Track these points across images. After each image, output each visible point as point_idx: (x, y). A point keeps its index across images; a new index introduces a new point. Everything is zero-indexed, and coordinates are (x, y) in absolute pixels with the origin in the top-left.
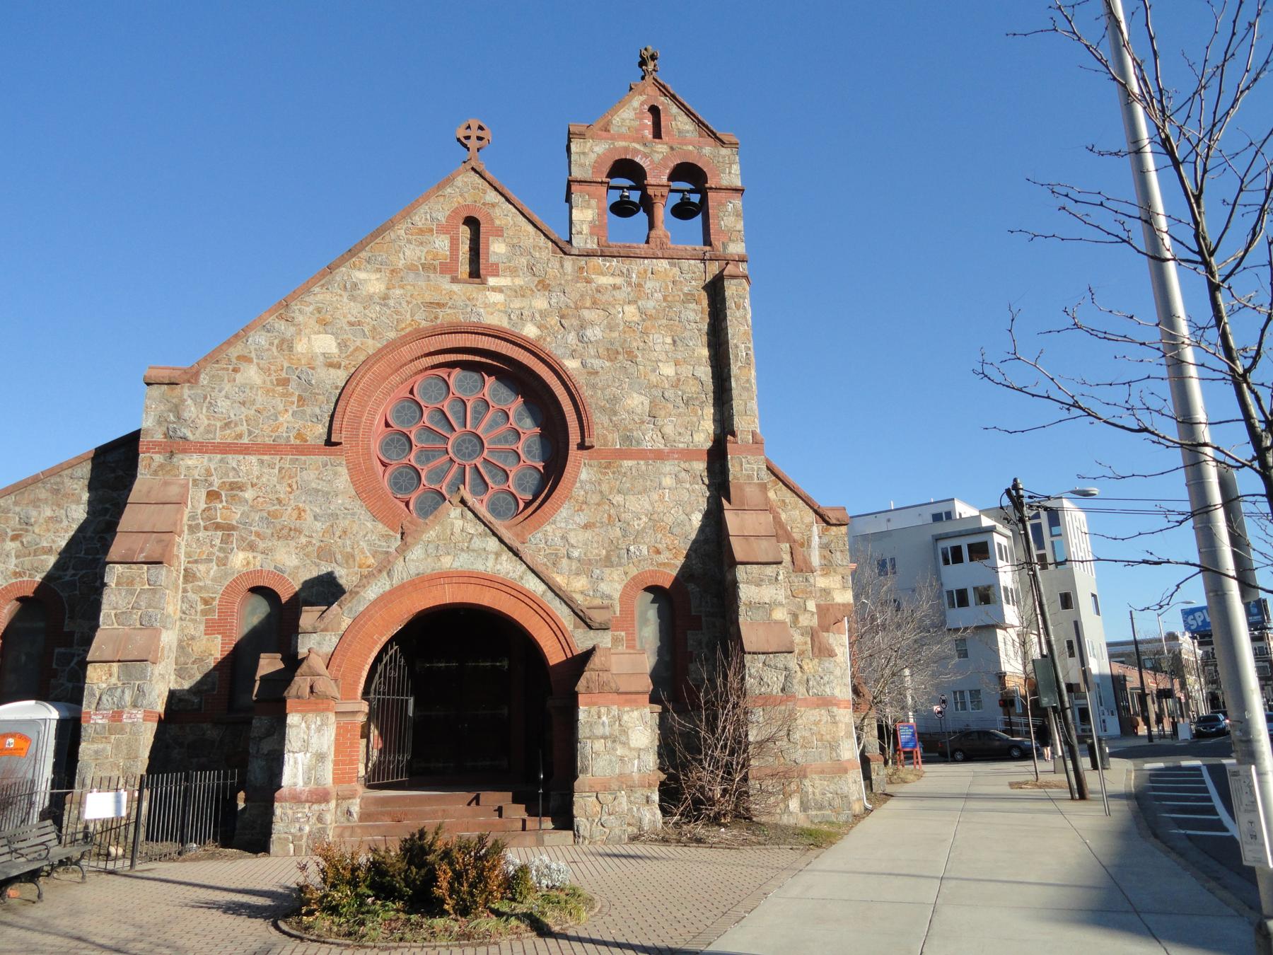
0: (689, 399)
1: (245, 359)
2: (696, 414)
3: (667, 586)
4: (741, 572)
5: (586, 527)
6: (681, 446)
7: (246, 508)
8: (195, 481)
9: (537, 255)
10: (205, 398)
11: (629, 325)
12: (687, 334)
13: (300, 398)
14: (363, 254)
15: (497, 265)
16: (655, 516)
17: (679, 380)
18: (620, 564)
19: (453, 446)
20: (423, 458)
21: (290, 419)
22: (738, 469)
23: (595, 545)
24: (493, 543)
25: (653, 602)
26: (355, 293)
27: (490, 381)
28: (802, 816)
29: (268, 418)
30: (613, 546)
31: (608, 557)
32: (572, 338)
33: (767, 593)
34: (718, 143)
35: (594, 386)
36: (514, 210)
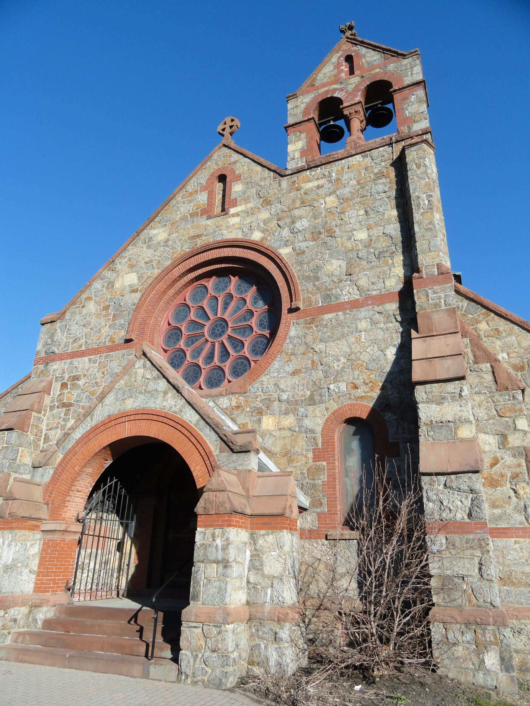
0: (380, 253)
1: (89, 299)
2: (387, 264)
3: (364, 416)
4: (420, 393)
5: (295, 373)
6: (374, 293)
7: (79, 391)
8: (56, 378)
9: (263, 183)
10: (66, 326)
11: (329, 211)
12: (378, 203)
13: (114, 315)
14: (157, 219)
15: (236, 199)
16: (353, 356)
17: (371, 240)
18: (321, 402)
19: (209, 331)
20: (190, 343)
21: (108, 330)
22: (424, 299)
23: (301, 388)
24: (163, 384)
25: (355, 434)
26: (150, 244)
27: (234, 280)
28: (503, 677)
29: (96, 332)
30: (316, 386)
31: (312, 397)
32: (286, 232)
33: (449, 411)
34: (400, 58)
35: (301, 263)
36: (249, 160)
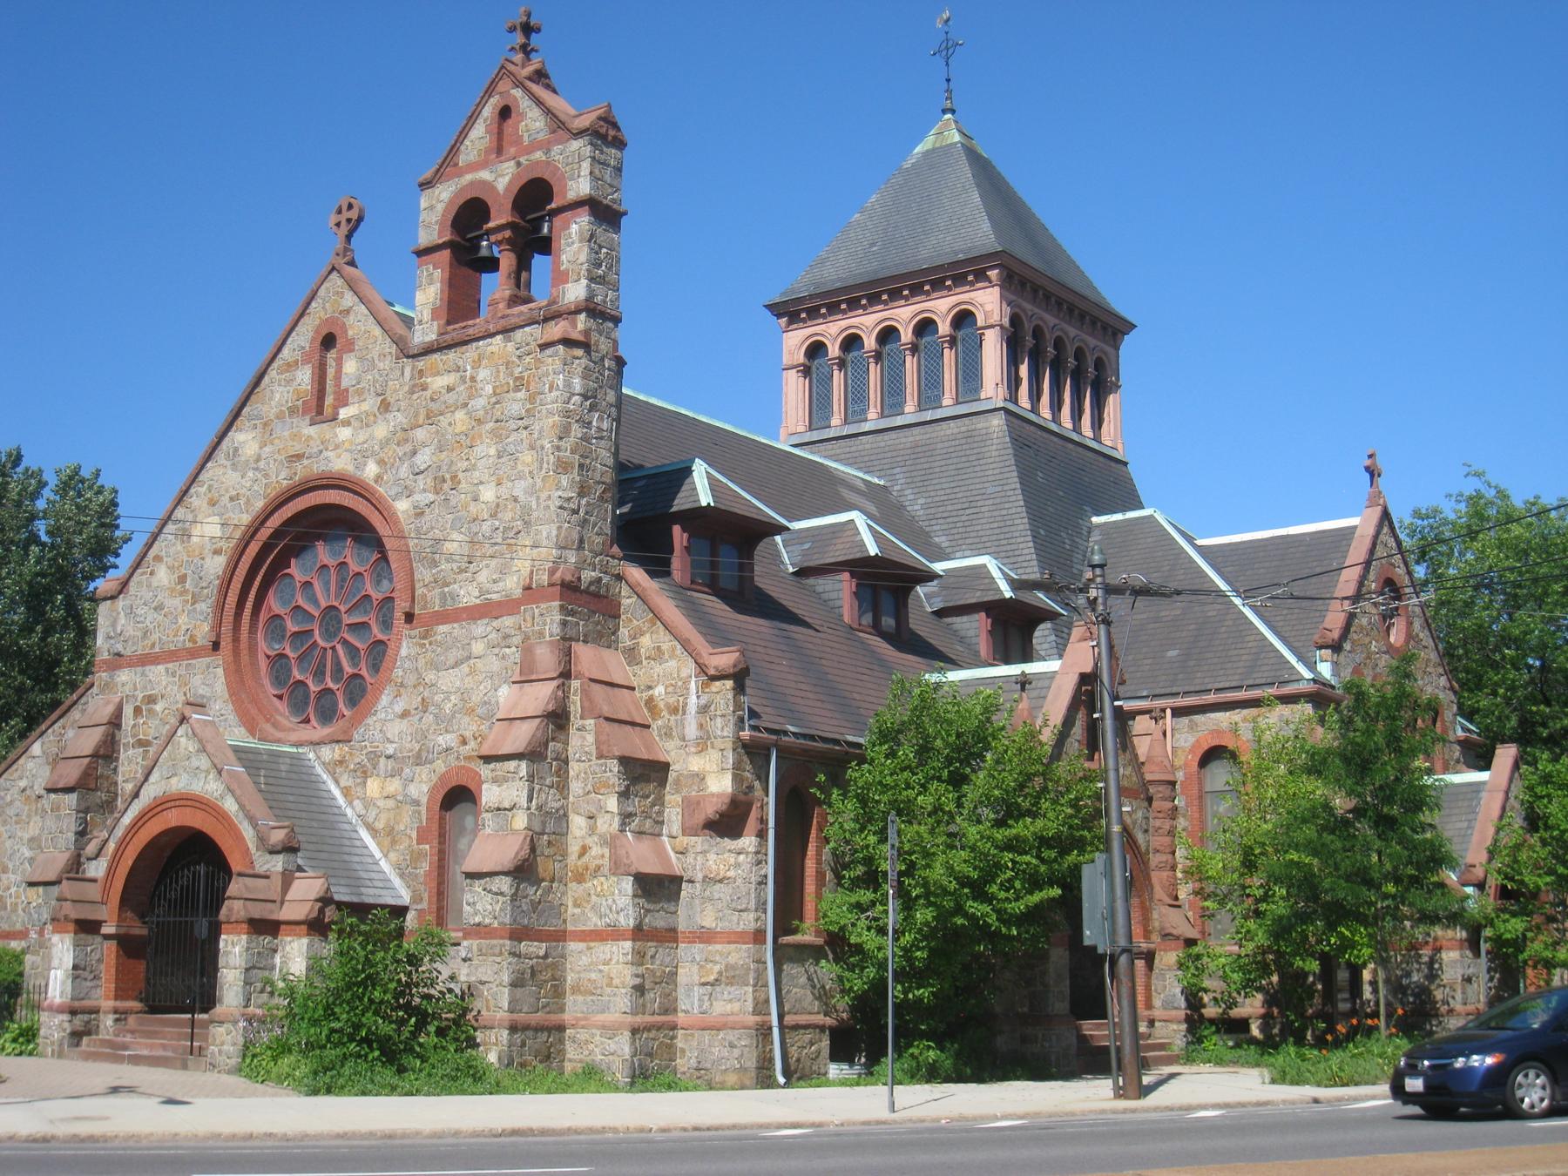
5: (405, 715)
15: (347, 390)
31: (419, 755)
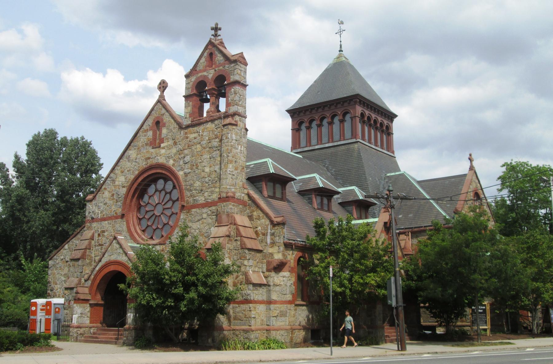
1: (105, 189)
35: (186, 181)
